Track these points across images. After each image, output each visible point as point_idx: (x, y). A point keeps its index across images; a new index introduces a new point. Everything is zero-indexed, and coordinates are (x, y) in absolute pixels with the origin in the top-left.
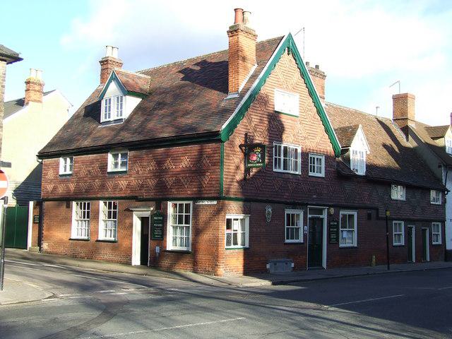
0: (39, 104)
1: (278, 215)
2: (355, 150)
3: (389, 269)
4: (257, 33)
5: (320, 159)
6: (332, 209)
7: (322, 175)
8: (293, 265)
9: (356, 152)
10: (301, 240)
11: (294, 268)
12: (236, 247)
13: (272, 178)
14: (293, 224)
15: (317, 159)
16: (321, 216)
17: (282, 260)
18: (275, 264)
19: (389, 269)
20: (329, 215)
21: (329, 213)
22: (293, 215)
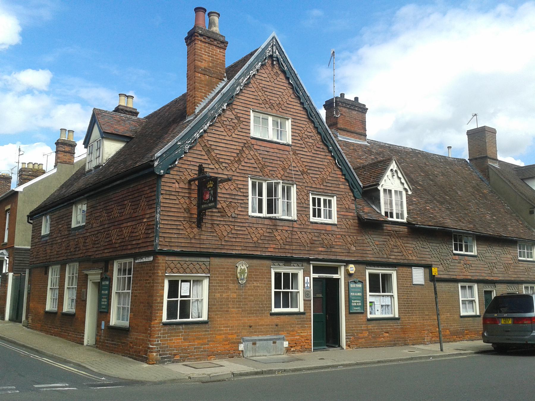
0: (371, 301)
1: (205, 72)
2: (388, 188)
3: (442, 350)
4: (226, 39)
5: (330, 201)
6: (352, 266)
7: (334, 220)
8: (286, 344)
9: (390, 191)
10: (301, 308)
11: (288, 350)
12: (325, 198)
13: (247, 225)
14: (287, 286)
15: (325, 201)
16: (335, 276)
17: (268, 337)
18: (254, 344)
19: (442, 350)
20: (349, 275)
21: (347, 271)
22: (286, 275)
